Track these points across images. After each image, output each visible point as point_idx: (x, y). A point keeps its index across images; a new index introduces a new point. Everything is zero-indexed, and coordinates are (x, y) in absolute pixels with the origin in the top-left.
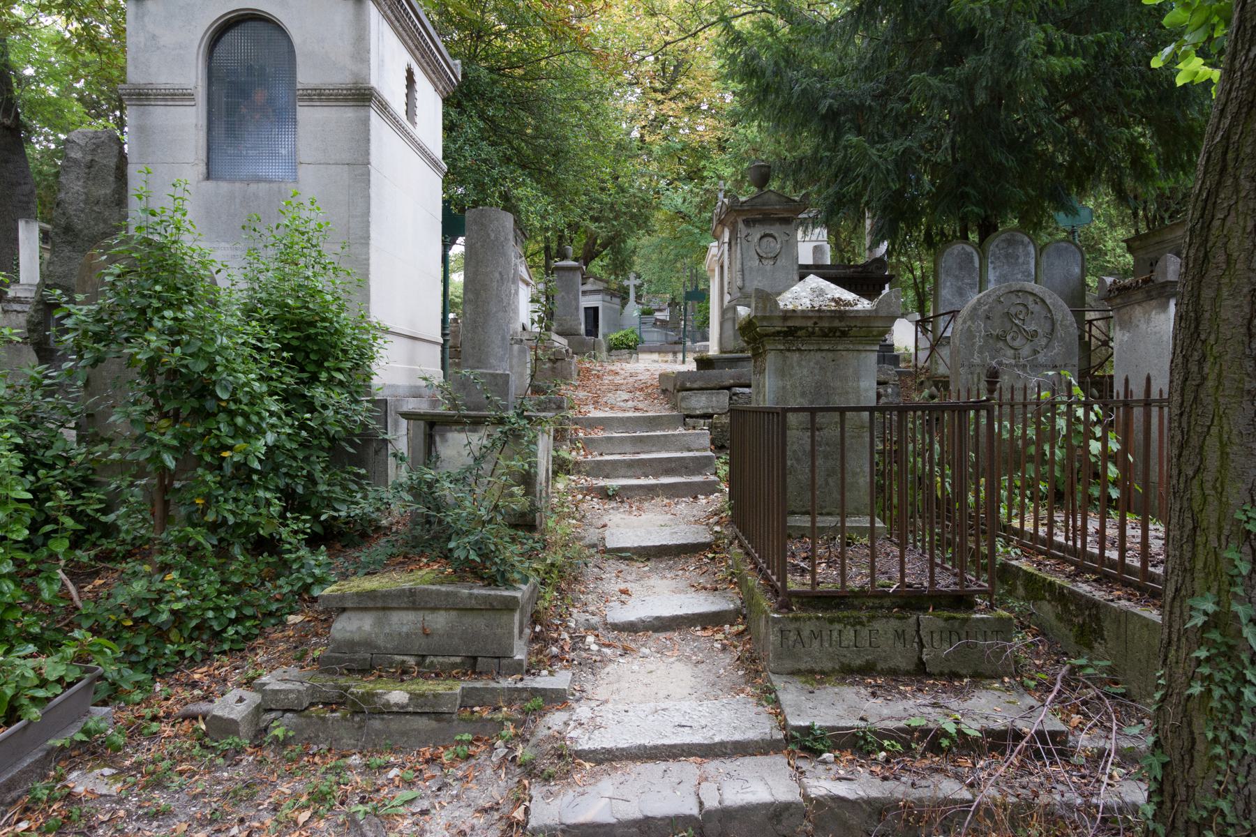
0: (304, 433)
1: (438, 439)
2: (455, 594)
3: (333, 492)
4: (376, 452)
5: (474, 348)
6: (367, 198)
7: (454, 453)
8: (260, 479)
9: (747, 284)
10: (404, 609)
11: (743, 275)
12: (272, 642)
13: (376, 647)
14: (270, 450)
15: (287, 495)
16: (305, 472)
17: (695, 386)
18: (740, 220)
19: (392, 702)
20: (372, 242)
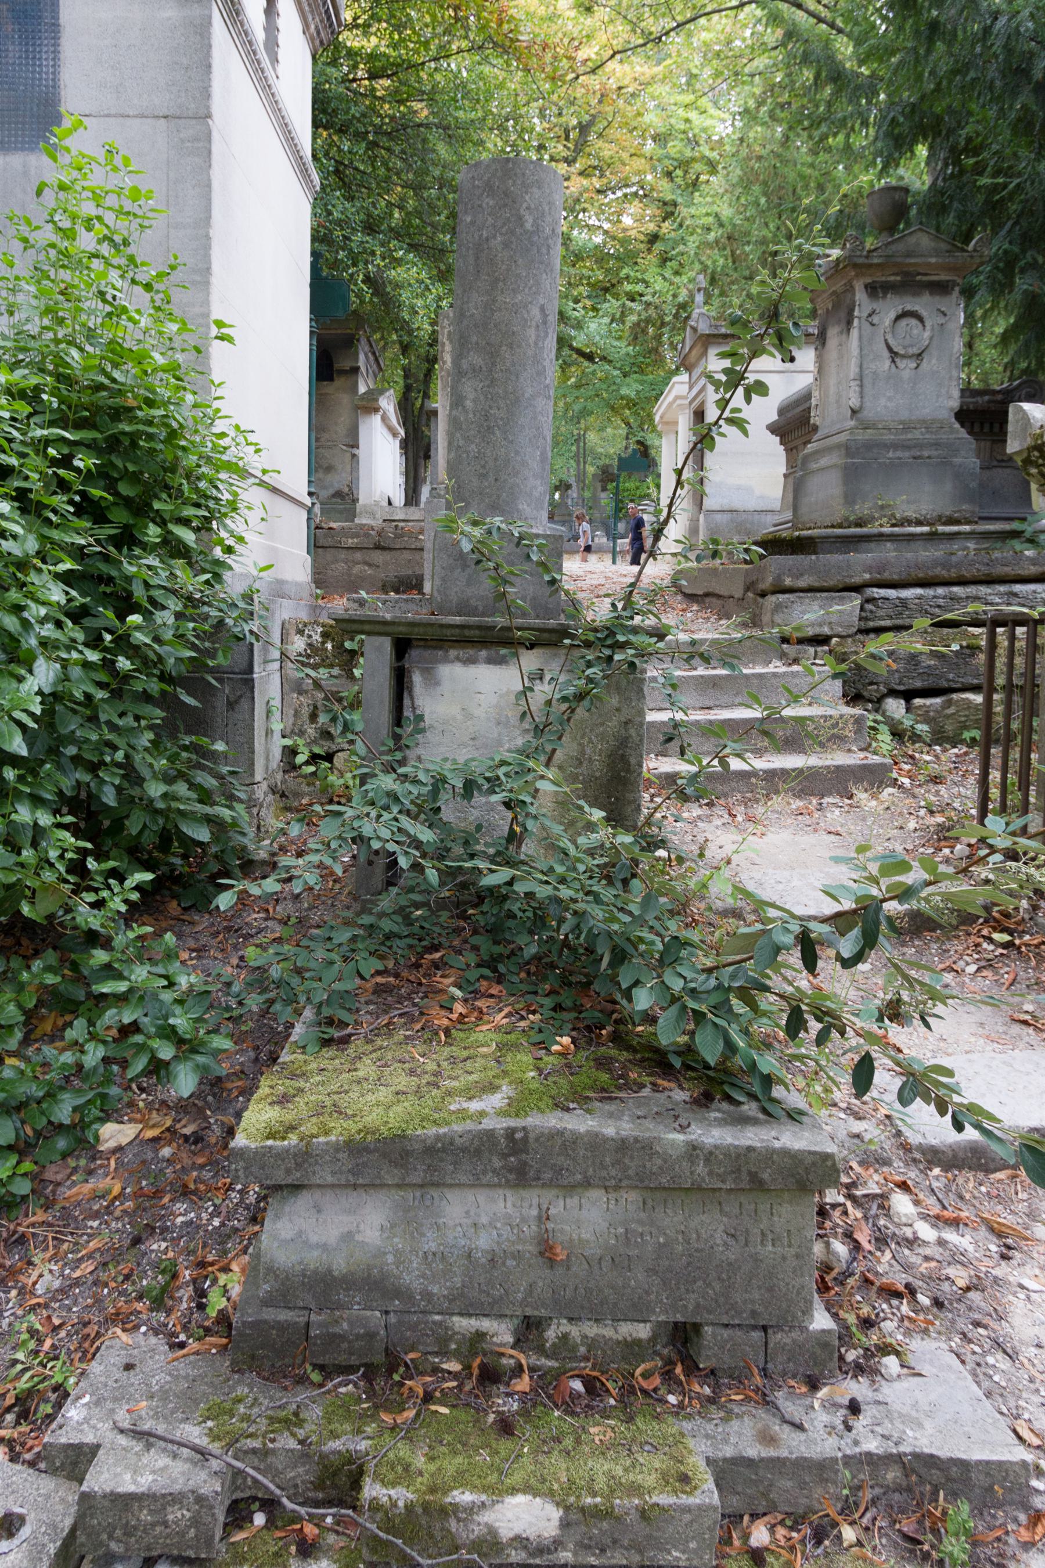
0: (124, 663)
1: (417, 678)
2: (647, 1147)
3: (176, 798)
4: (231, 705)
5: (483, 476)
6: (208, 186)
7: (455, 710)
8: (21, 779)
9: (868, 404)
11: (861, 386)
14: (52, 699)
15: (85, 813)
16: (120, 756)
17: (802, 583)
18: (859, 286)
19: (506, 1533)
20: (214, 280)
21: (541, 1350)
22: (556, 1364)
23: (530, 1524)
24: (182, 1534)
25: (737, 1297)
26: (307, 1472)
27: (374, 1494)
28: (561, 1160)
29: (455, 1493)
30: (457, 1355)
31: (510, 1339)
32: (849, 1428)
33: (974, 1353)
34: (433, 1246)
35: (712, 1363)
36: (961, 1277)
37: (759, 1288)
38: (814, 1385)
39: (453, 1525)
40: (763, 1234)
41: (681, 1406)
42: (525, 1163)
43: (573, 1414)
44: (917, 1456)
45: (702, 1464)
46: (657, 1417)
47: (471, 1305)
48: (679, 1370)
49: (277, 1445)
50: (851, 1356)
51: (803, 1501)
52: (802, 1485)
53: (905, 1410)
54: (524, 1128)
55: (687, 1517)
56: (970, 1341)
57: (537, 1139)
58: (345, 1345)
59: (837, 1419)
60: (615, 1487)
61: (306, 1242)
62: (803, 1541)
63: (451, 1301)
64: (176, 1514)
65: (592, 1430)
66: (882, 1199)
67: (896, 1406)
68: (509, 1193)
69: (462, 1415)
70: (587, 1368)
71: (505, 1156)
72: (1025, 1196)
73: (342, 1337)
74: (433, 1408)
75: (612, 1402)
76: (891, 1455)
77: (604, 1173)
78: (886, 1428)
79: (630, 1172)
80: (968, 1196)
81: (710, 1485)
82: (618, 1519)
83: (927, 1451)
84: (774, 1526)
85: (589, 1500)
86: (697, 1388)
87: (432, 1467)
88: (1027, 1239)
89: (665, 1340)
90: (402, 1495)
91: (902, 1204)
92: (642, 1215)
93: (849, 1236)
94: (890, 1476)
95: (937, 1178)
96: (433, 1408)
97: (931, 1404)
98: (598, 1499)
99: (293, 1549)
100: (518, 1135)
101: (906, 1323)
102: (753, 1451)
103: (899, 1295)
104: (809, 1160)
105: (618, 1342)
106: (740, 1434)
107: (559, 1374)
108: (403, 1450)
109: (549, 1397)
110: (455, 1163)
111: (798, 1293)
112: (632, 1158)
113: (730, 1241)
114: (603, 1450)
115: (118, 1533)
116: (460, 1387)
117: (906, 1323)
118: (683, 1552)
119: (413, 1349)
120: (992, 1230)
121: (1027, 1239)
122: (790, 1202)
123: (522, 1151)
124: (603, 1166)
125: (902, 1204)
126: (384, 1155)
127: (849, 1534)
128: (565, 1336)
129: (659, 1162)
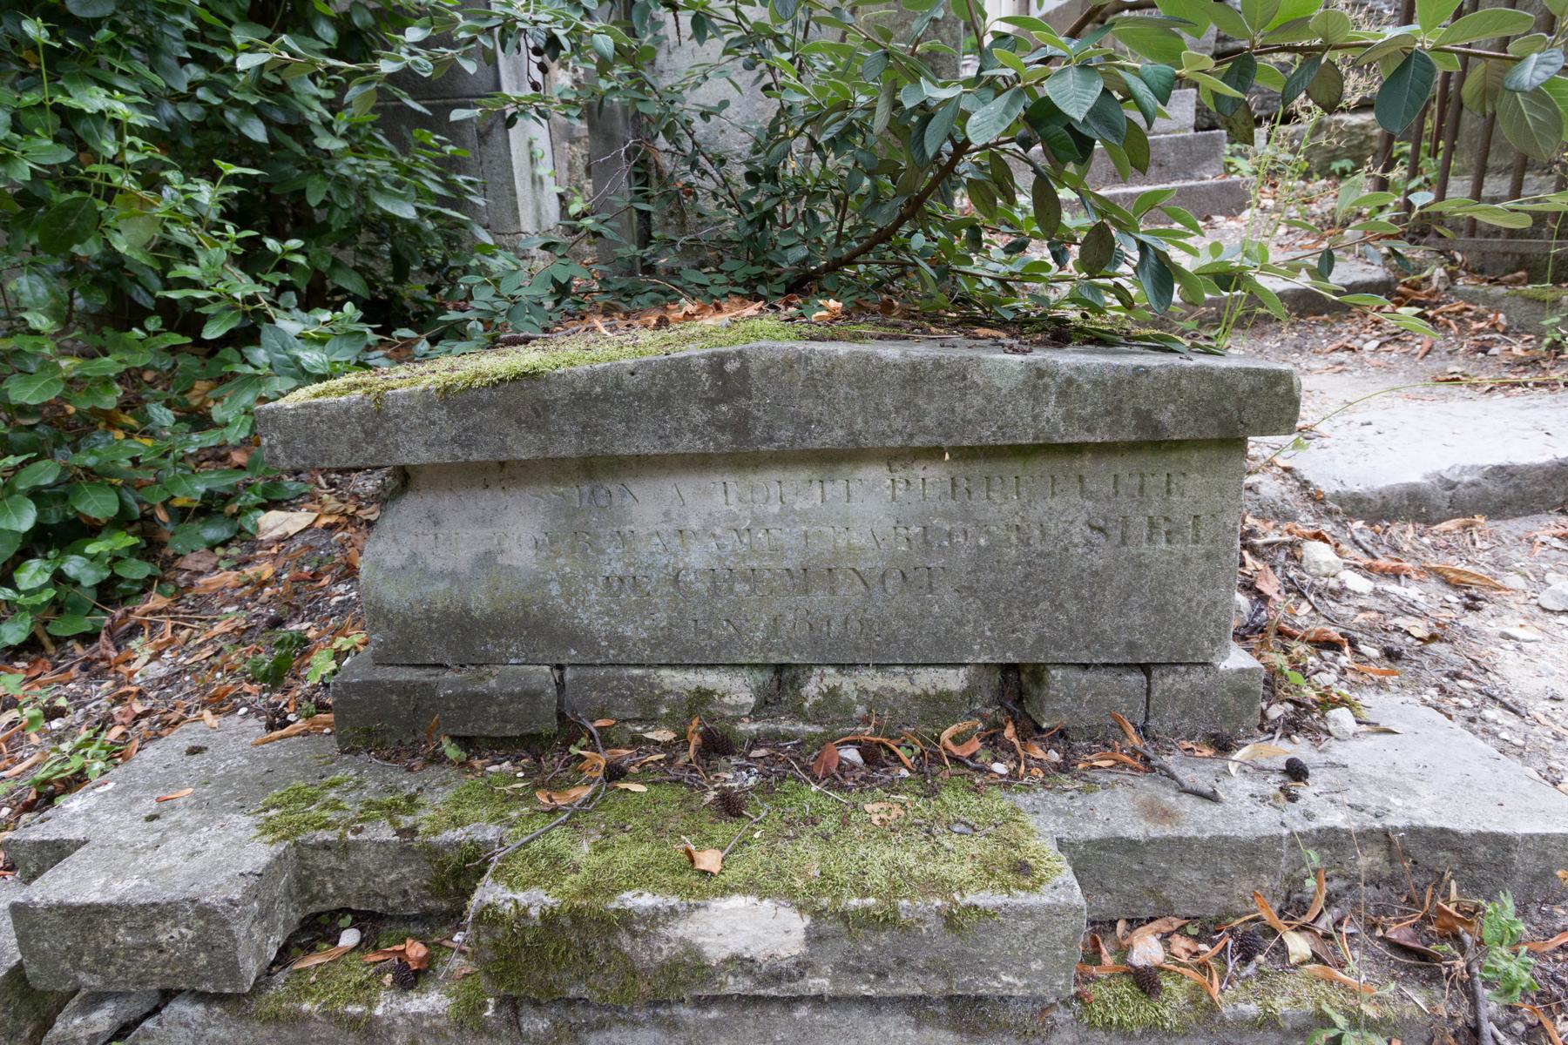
2: (958, 376)
10: (700, 463)
12: (203, 602)
13: (573, 638)
19: (715, 952)
21: (798, 713)
22: (820, 730)
23: (755, 938)
24: (188, 961)
25: (1106, 624)
26: (416, 873)
27: (490, 899)
28: (808, 406)
29: (627, 895)
30: (669, 721)
31: (748, 699)
32: (1292, 798)
33: (1461, 707)
34: (618, 568)
35: (1064, 720)
36: (1420, 629)
37: (1143, 608)
38: (1223, 746)
39: (626, 942)
40: (1152, 525)
41: (1013, 775)
42: (747, 414)
43: (841, 788)
44: (1414, 832)
45: (1051, 848)
46: (976, 790)
47: (686, 652)
48: (1009, 732)
49: (362, 837)
50: (1276, 712)
51: (1217, 900)
52: (1218, 878)
53: (1378, 774)
54: (740, 353)
55: (1028, 925)
56: (1451, 695)
57: (764, 372)
58: (494, 709)
59: (1272, 785)
60: (900, 880)
61: (424, 571)
62: (1221, 957)
63: (654, 648)
64: (166, 934)
65: (868, 808)
66: (1293, 550)
67: (1362, 769)
68: (731, 480)
69: (666, 793)
70: (867, 732)
71: (711, 403)
72: (1486, 545)
73: (489, 698)
74: (622, 786)
75: (905, 773)
76: (1372, 831)
77: (883, 426)
78: (1355, 796)
79: (927, 421)
80: (1406, 548)
81: (1067, 875)
82: (905, 929)
83: (1434, 823)
84: (1169, 935)
85: (855, 902)
86: (1039, 753)
87: (597, 861)
88: (1498, 588)
89: (988, 697)
90: (538, 900)
91: (1318, 554)
92: (951, 504)
93: (1249, 587)
94: (1363, 862)
95: (1361, 531)
96: (622, 786)
97: (1406, 766)
98: (871, 901)
99: (388, 978)
100: (731, 366)
101: (1350, 675)
102: (1136, 829)
103: (1334, 646)
104: (1244, 385)
105: (917, 698)
106: (1112, 809)
107: (822, 742)
108: (559, 840)
109: (805, 769)
110: (628, 420)
111: (1206, 613)
112: (930, 396)
113: (1096, 537)
114: (885, 833)
115: (87, 960)
116: (670, 761)
117: (1350, 675)
118: (1020, 976)
119: (602, 715)
120: (1447, 582)
121: (1498, 588)
122: (1201, 471)
123: (739, 393)
124: (881, 414)
125: (1318, 554)
126: (508, 411)
127: (1299, 946)
128: (833, 692)
129: (978, 401)
